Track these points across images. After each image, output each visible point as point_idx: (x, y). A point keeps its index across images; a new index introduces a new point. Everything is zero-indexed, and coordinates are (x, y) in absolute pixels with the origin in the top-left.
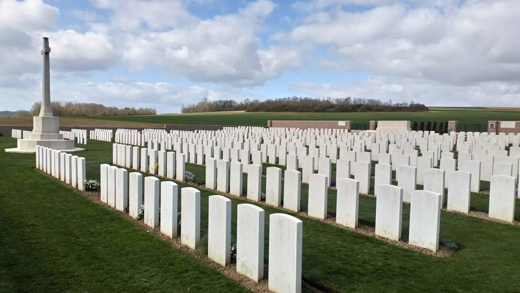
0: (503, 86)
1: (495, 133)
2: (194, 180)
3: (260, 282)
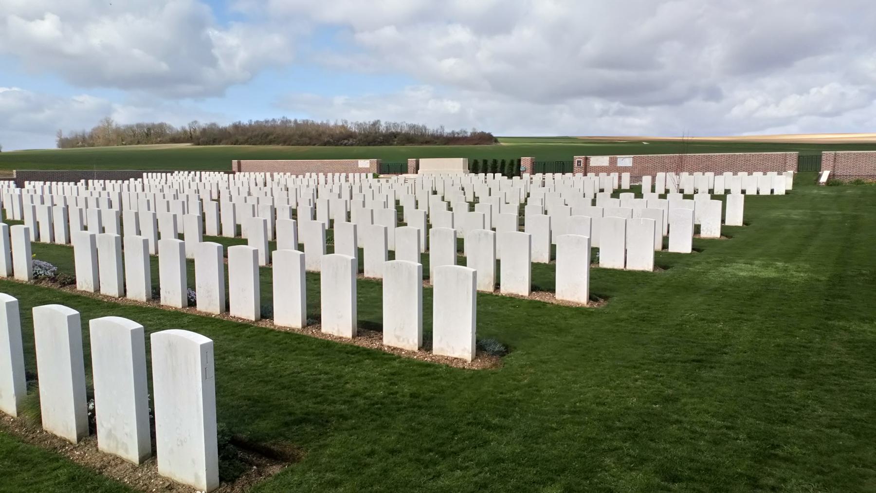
0: (598, 104)
2: (54, 276)
3: (143, 462)
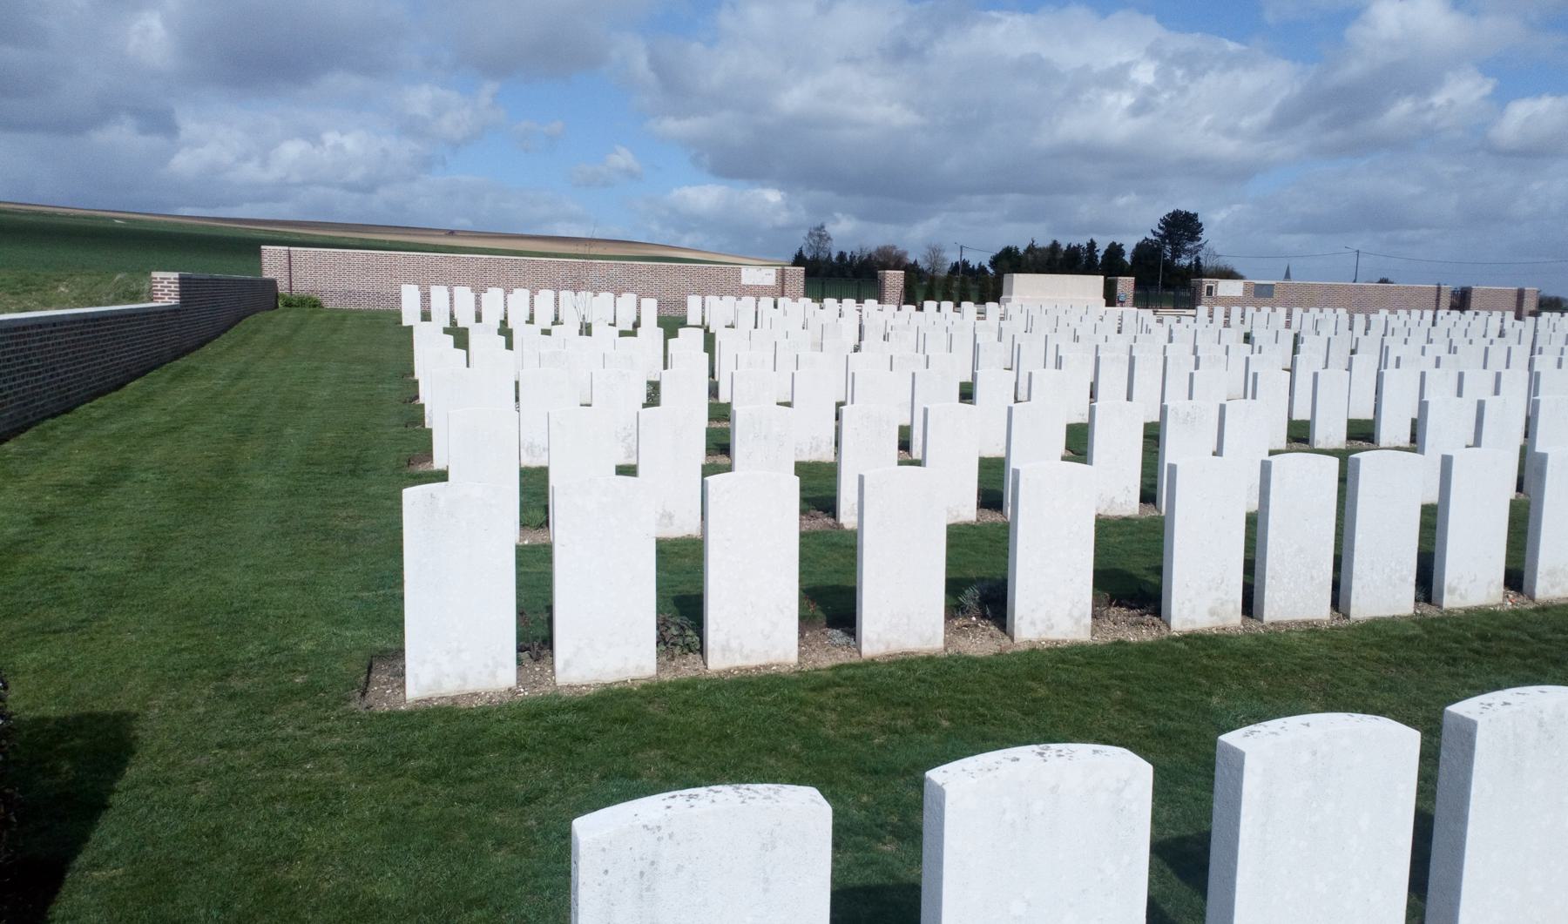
1: (895, 307)
